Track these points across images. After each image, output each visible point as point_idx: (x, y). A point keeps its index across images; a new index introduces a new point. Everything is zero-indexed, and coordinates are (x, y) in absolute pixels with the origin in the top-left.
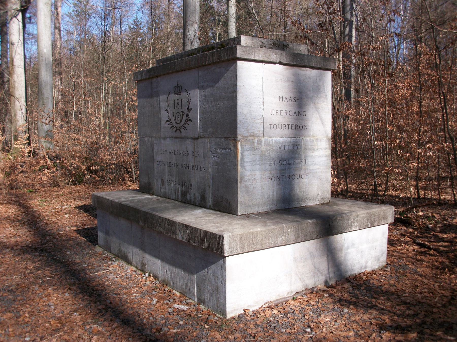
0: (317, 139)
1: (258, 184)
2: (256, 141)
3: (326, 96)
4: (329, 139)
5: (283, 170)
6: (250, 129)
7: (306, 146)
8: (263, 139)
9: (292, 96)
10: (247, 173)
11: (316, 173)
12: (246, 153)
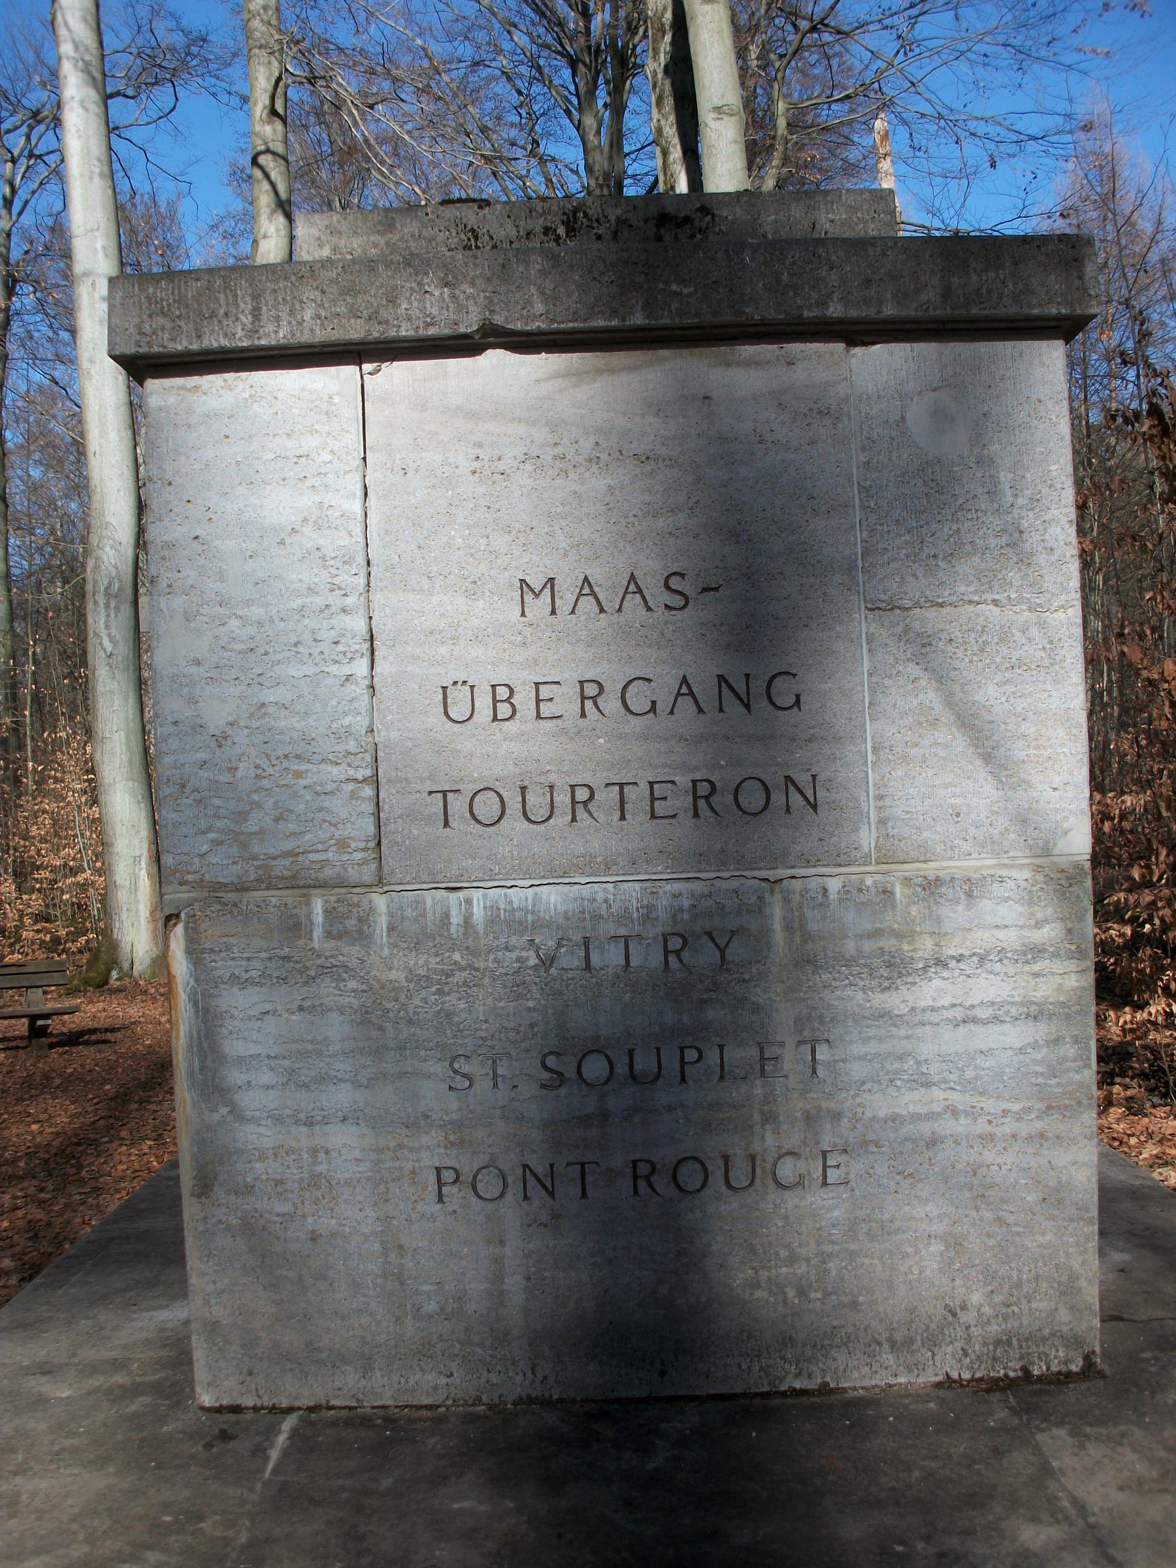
0: (932, 886)
1: (353, 1218)
2: (318, 916)
3: (1015, 538)
4: (1061, 880)
5: (584, 1120)
6: (260, 834)
7: (807, 937)
8: (380, 902)
9: (651, 569)
10: (258, 1135)
11: (933, 1142)
12: (238, 1002)
